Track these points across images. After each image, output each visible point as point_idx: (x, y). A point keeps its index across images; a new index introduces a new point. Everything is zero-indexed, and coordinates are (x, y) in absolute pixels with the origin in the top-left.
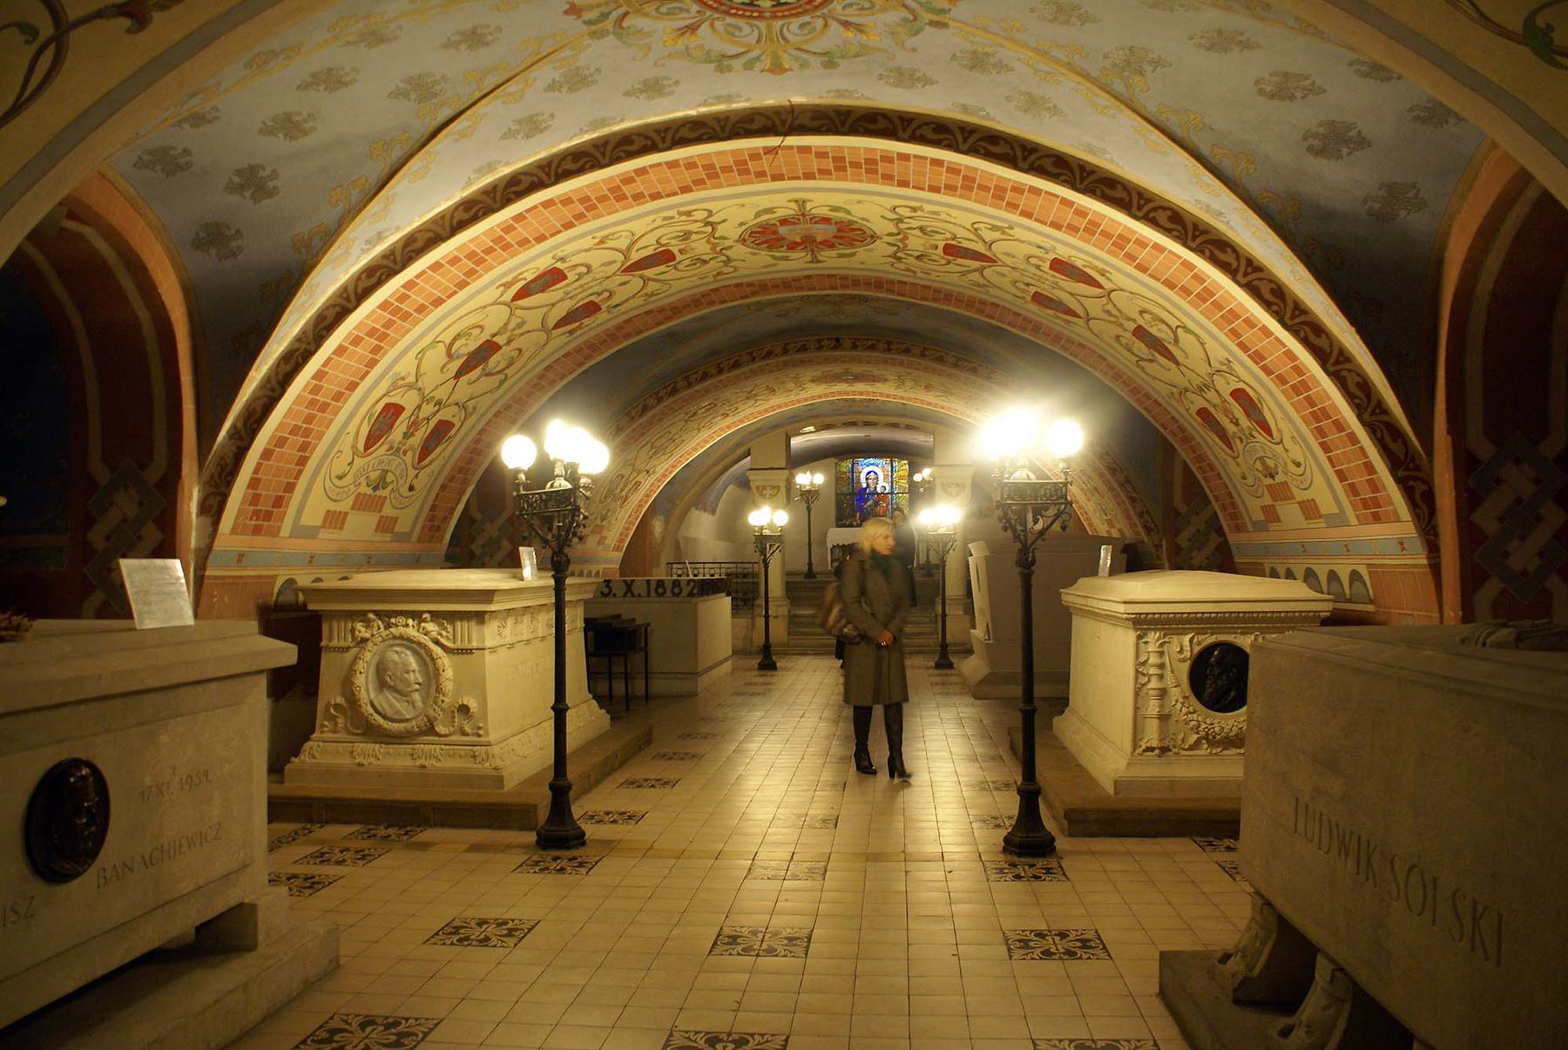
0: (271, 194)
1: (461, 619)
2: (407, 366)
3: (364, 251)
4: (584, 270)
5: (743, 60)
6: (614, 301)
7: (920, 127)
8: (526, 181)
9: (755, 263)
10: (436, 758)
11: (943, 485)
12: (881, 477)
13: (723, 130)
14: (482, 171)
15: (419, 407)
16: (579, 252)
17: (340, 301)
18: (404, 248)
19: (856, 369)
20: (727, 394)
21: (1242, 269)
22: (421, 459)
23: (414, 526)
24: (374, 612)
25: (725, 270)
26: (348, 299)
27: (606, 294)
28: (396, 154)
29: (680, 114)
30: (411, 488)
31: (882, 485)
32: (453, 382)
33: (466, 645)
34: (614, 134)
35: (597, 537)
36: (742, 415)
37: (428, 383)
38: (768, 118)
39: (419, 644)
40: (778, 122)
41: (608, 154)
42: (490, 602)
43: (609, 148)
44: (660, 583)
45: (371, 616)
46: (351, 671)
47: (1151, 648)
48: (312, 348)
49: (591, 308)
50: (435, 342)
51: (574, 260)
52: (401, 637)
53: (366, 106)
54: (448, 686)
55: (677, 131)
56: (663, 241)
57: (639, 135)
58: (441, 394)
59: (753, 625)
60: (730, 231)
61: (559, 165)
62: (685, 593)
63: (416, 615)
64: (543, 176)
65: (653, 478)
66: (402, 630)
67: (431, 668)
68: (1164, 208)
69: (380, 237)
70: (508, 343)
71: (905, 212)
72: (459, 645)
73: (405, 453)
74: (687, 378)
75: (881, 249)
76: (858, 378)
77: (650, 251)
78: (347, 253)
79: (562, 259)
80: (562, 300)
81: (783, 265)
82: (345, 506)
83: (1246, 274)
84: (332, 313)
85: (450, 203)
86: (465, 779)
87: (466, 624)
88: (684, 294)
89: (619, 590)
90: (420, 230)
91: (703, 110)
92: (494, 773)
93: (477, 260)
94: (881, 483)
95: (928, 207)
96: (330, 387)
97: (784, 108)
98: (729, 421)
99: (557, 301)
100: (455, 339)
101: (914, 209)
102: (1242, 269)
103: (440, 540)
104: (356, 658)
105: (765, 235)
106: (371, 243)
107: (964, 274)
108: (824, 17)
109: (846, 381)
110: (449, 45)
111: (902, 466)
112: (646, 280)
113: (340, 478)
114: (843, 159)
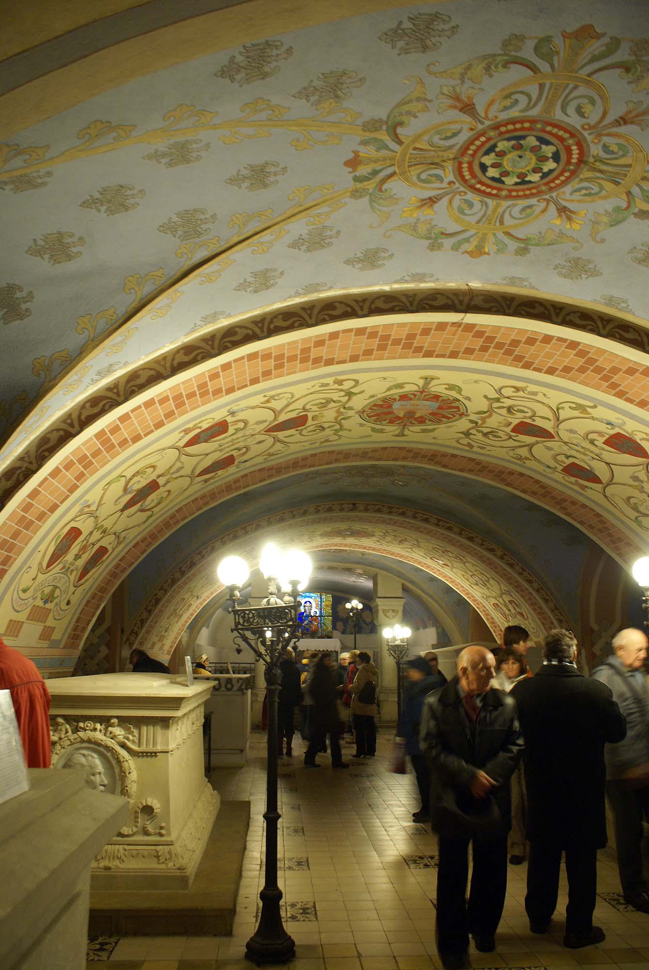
0: (21, 316)
1: (147, 724)
2: (93, 497)
4: (241, 425)
5: (454, 240)
7: (568, 314)
8: (241, 333)
10: (119, 858)
11: (384, 611)
12: (314, 605)
13: (411, 303)
14: (206, 320)
15: (91, 533)
16: (248, 408)
17: (64, 426)
18: (128, 381)
19: (357, 526)
22: (80, 578)
23: (62, 638)
24: (65, 717)
26: (72, 425)
28: (148, 289)
29: (376, 288)
30: (68, 603)
31: (314, 610)
32: (119, 513)
33: (151, 748)
34: (319, 301)
37: (103, 513)
38: (448, 298)
39: (107, 747)
40: (457, 302)
41: (314, 317)
42: (177, 708)
43: (315, 312)
45: (60, 720)
48: (33, 467)
49: (229, 461)
51: (241, 416)
52: (89, 741)
53: (130, 241)
54: (133, 788)
55: (372, 302)
56: (308, 407)
57: (340, 303)
58: (107, 524)
60: (359, 403)
61: (271, 322)
63: (105, 721)
64: (257, 330)
66: (90, 734)
67: (117, 771)
69: (110, 370)
70: (164, 485)
71: (507, 392)
72: (144, 748)
73: (72, 572)
75: (463, 424)
76: (354, 534)
77: (293, 415)
78: (80, 380)
79: (233, 414)
80: (215, 451)
82: (22, 617)
84: (54, 437)
85: (172, 346)
86: (151, 880)
87: (151, 728)
88: (354, 446)
90: (143, 368)
91: (396, 286)
92: (178, 873)
94: (314, 610)
95: (532, 388)
96: (39, 506)
97: (460, 290)
99: (211, 451)
100: (134, 476)
101: (517, 389)
105: (381, 411)
106: (101, 374)
107: (514, 448)
108: (548, 201)
110: (235, 180)
112: (277, 440)
113: (24, 591)
114: (85, 457)
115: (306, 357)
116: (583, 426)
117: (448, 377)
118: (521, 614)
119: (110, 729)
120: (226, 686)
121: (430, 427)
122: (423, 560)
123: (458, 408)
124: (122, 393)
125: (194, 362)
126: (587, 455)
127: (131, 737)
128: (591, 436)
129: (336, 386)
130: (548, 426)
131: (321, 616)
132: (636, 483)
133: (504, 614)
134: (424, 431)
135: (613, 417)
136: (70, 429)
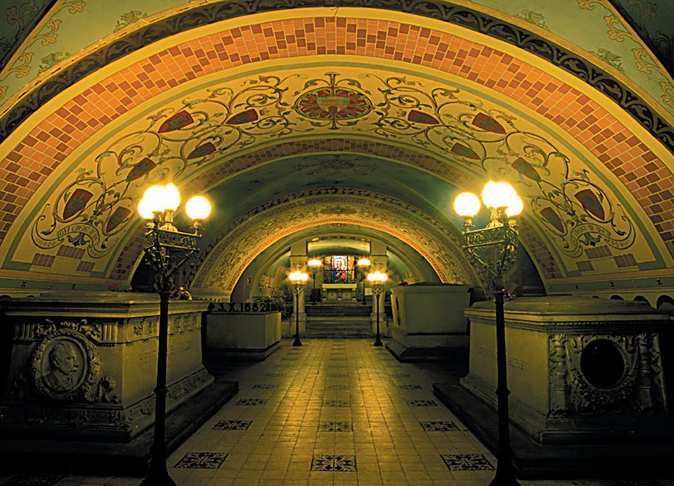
3: (43, 69)
6: (223, 145)
9: (301, 125)
15: (103, 196)
17: (27, 104)
20: (282, 216)
21: (624, 98)
25: (286, 131)
27: (218, 139)
30: (103, 247)
31: (344, 267)
35: (219, 283)
36: (288, 229)
37: (108, 179)
44: (248, 305)
46: (31, 358)
47: (557, 343)
50: (109, 152)
51: (197, 108)
59: (291, 325)
60: (289, 98)
62: (260, 309)
65: (246, 256)
68: (574, 59)
70: (161, 163)
71: (393, 83)
73: (96, 224)
74: (263, 206)
75: (373, 116)
76: (342, 211)
81: (317, 130)
82: (53, 252)
83: (627, 101)
89: (227, 308)
90: (85, 60)
93: (130, 91)
94: (343, 266)
95: (409, 78)
98: (282, 230)
102: (624, 98)
103: (126, 278)
104: (36, 348)
105: (309, 104)
109: (336, 213)
111: (352, 259)
112: (241, 132)
115: (220, 52)
116: (456, 110)
117: (353, 73)
118: (453, 263)
119: (82, 327)
120: (253, 309)
121: (353, 120)
122: (391, 229)
123: (364, 101)
124: (69, 79)
125: (123, 53)
126: (464, 136)
127: (95, 333)
128: (463, 118)
129: (263, 83)
130: (431, 112)
131: (347, 270)
132: (502, 156)
133: (443, 264)
134: (350, 124)
135: (472, 99)
136: (31, 106)
